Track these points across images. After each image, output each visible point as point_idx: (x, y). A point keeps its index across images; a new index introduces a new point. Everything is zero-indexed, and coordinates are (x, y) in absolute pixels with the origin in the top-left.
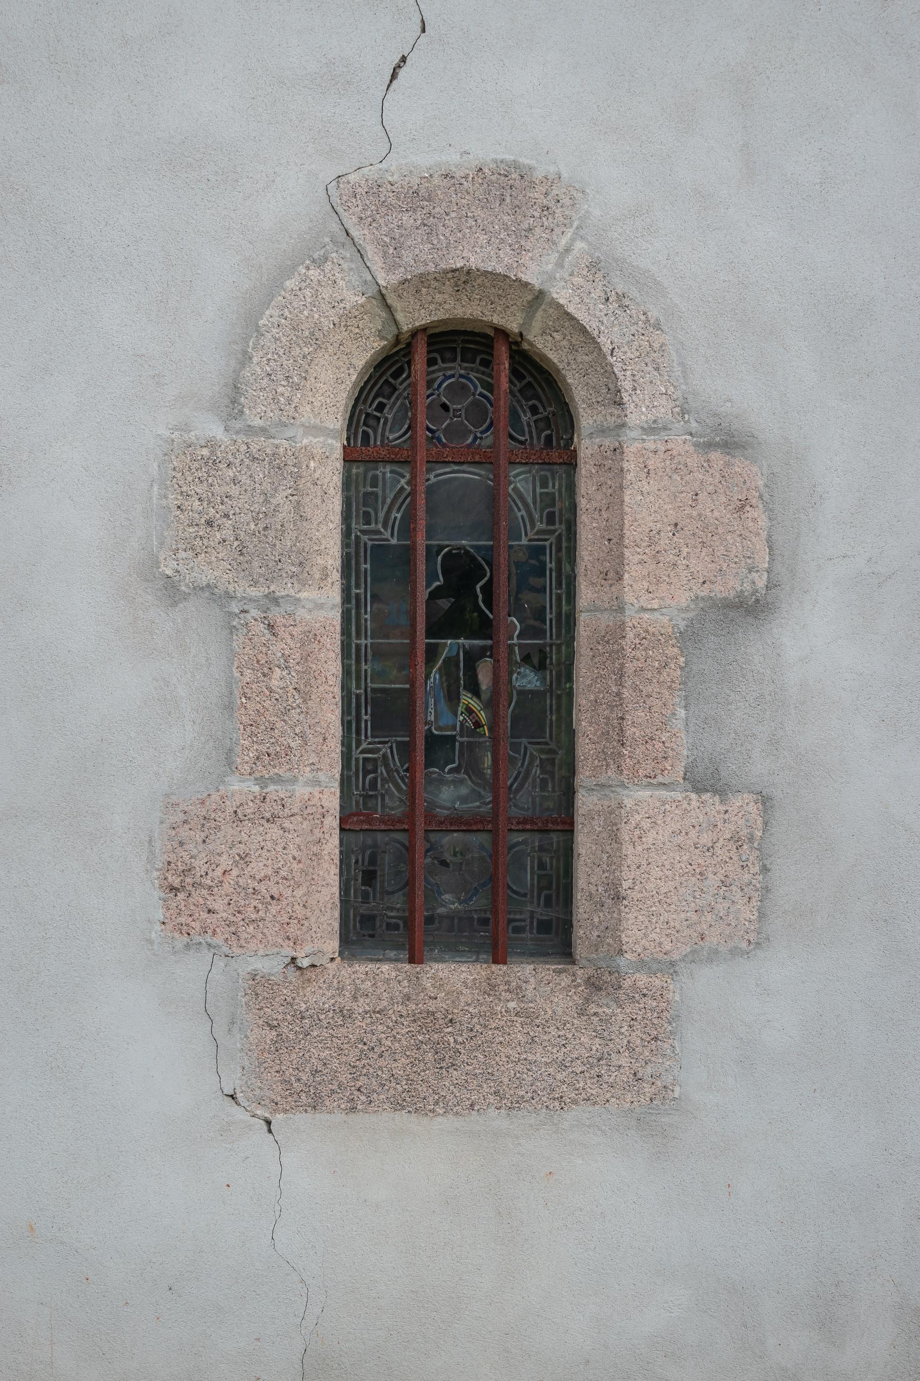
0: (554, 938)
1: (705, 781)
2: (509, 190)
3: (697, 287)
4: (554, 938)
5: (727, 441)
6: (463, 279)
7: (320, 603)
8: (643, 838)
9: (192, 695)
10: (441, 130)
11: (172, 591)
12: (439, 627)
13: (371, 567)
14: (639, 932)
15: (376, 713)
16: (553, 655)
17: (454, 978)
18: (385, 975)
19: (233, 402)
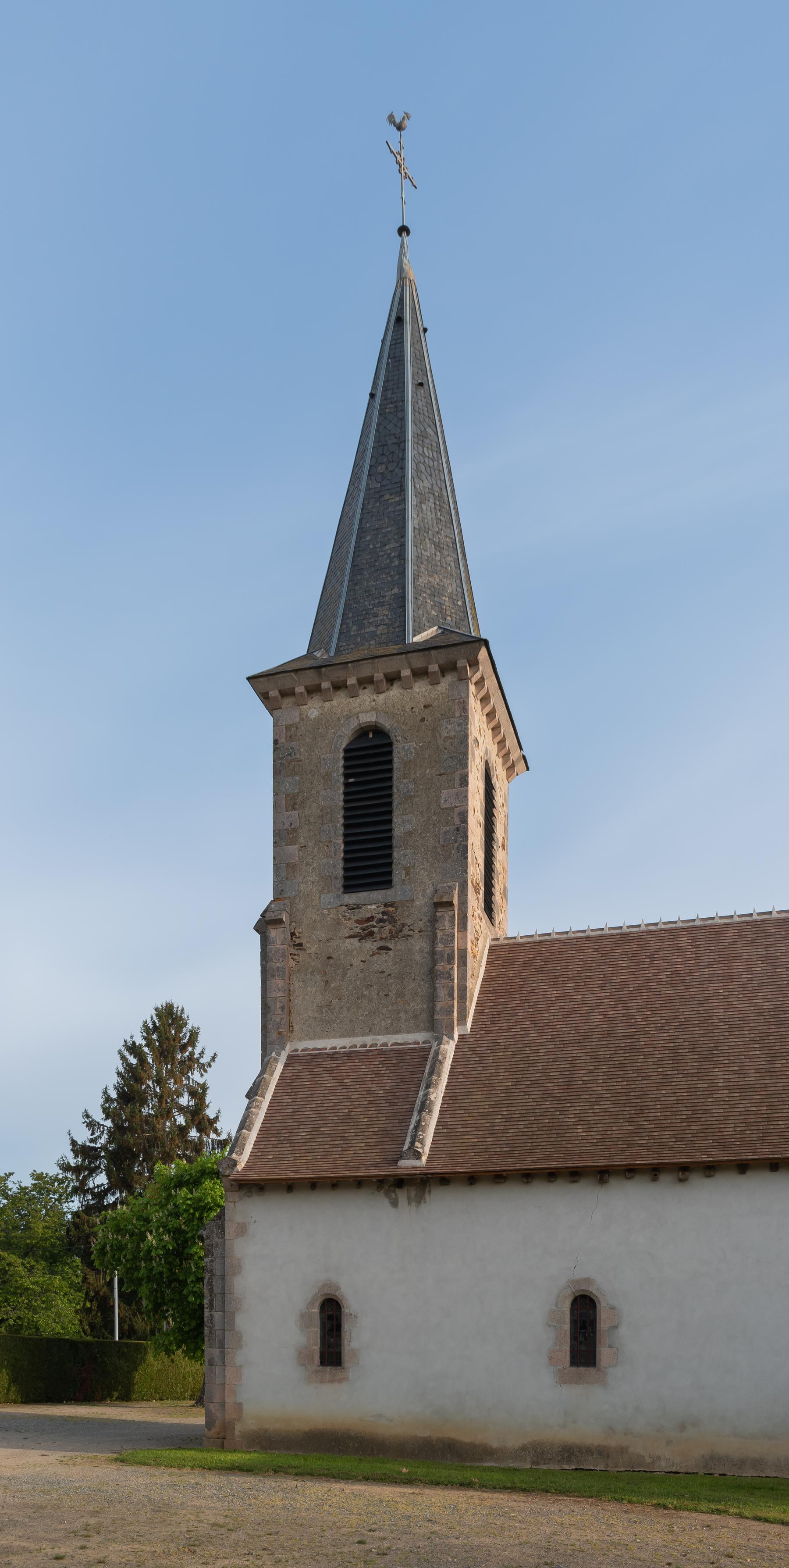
0: (340, 1365)
1: (610, 1347)
2: (588, 1280)
3: (610, 1292)
4: (340, 1365)
5: (613, 1308)
6: (583, 1290)
7: (567, 1327)
8: (603, 1353)
9: (556, 1338)
10: (579, 1274)
11: (550, 1326)
12: (581, 1328)
13: (573, 1322)
14: (346, 1365)
15: (574, 1338)
16: (594, 1332)
17: (582, 1369)
18: (574, 1369)
19: (557, 1305)
